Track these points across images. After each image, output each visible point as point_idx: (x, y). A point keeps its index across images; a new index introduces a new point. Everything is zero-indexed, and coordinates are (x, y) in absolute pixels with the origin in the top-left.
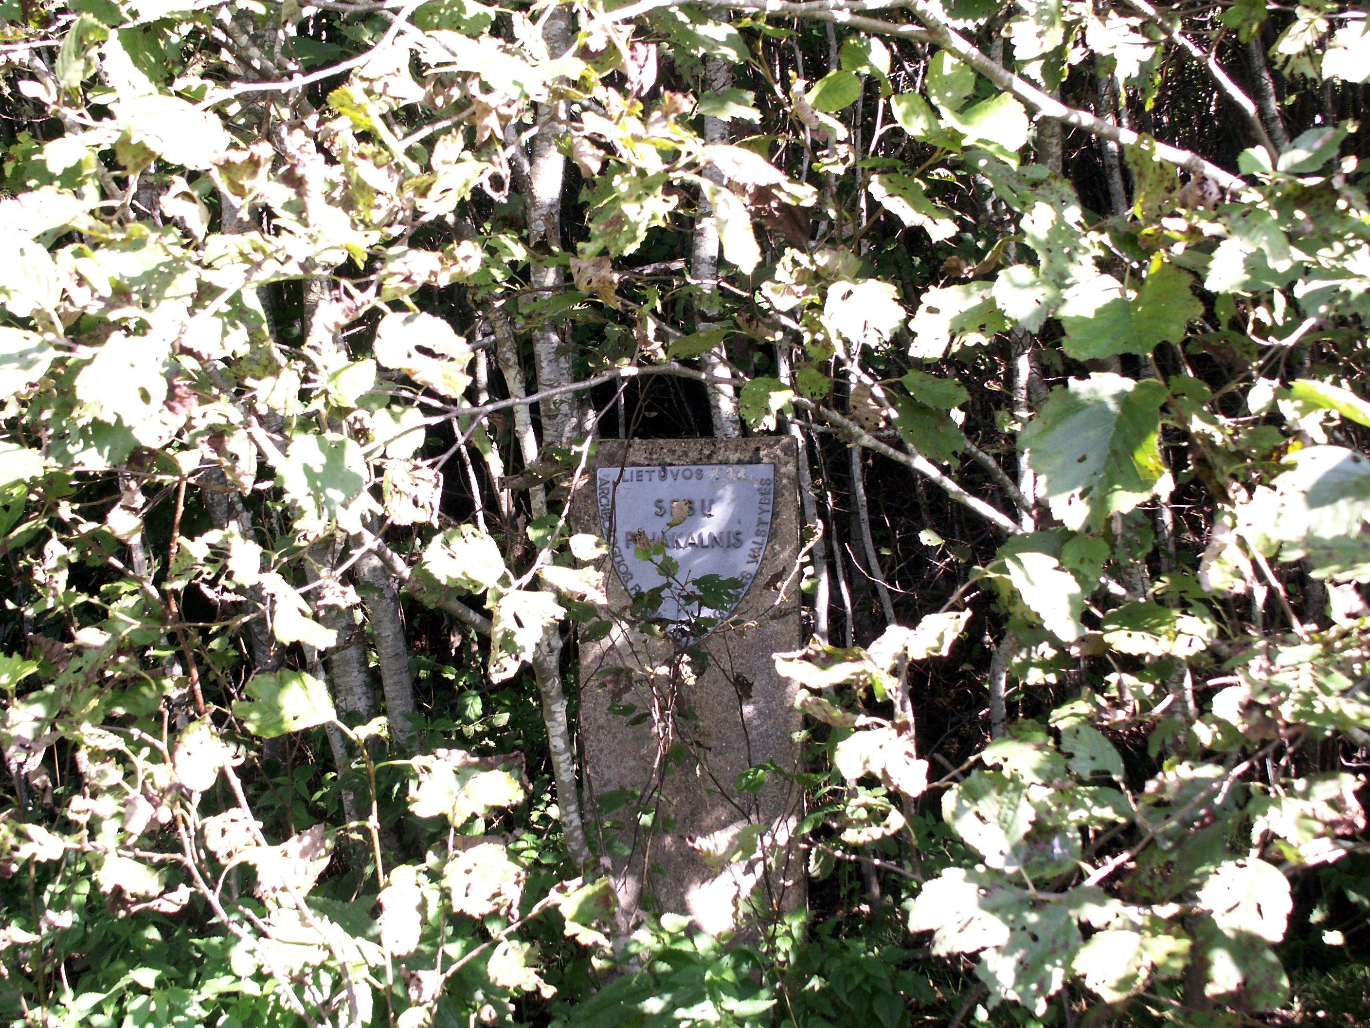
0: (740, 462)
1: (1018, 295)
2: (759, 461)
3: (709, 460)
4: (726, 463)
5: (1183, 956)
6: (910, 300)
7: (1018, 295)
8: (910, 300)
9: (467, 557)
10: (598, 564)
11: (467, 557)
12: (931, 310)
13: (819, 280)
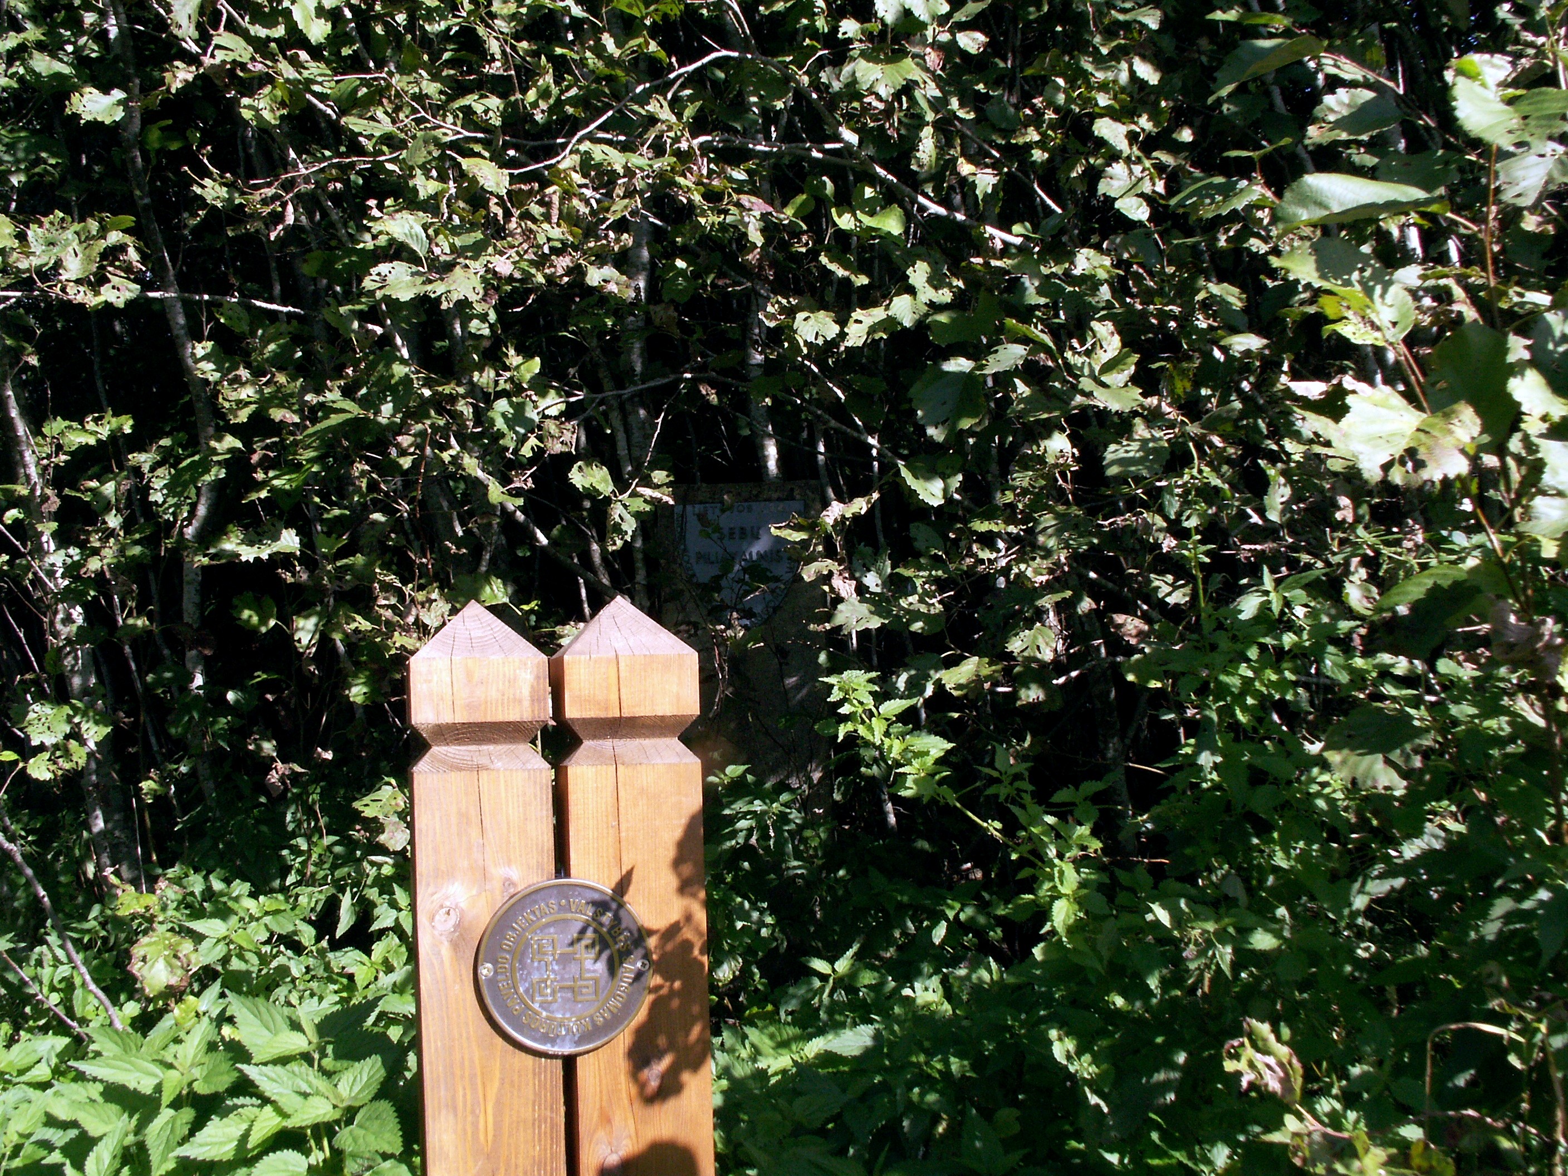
0: (779, 499)
1: (903, 310)
2: (793, 499)
3: (756, 498)
4: (769, 500)
5: (1451, 657)
6: (842, 321)
7: (903, 310)
8: (842, 321)
9: (589, 478)
10: (668, 485)
11: (589, 478)
12: (857, 321)
13: (791, 312)
